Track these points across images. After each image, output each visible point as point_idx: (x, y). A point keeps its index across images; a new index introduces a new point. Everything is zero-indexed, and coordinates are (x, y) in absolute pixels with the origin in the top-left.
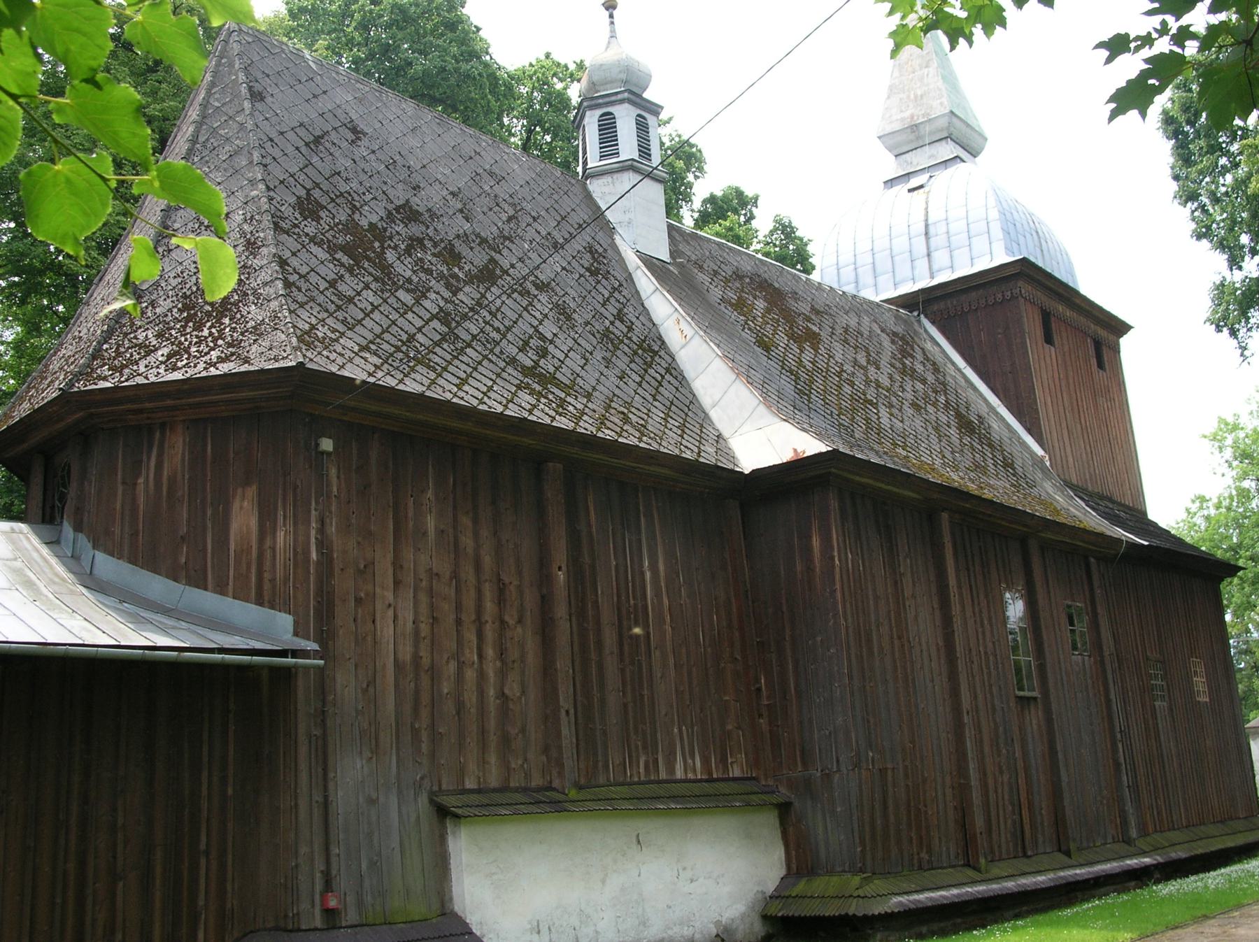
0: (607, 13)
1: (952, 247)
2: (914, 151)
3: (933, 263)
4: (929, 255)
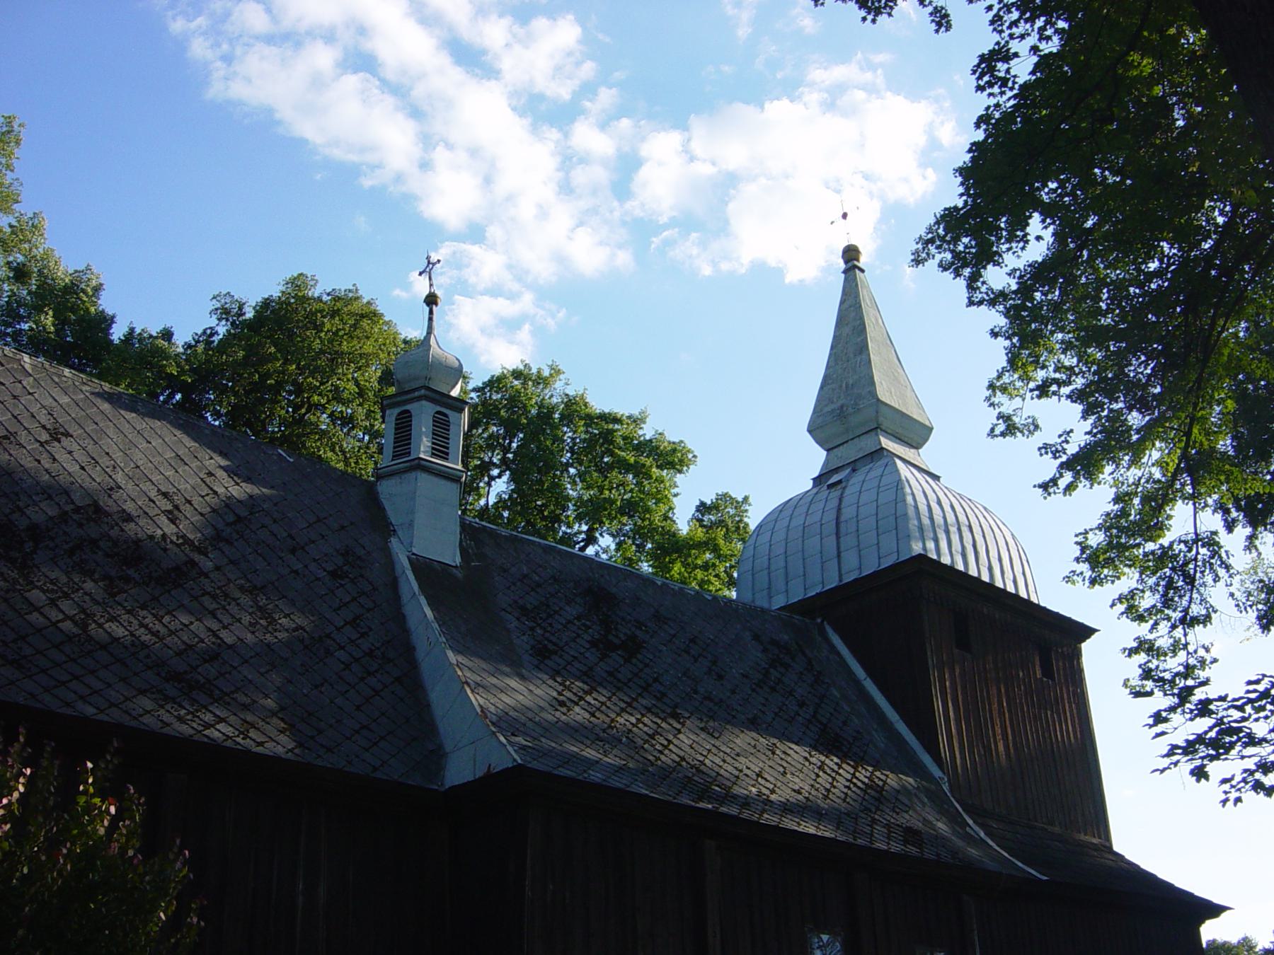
0: (427, 309)
1: (861, 546)
2: (845, 445)
3: (842, 565)
4: (839, 556)
